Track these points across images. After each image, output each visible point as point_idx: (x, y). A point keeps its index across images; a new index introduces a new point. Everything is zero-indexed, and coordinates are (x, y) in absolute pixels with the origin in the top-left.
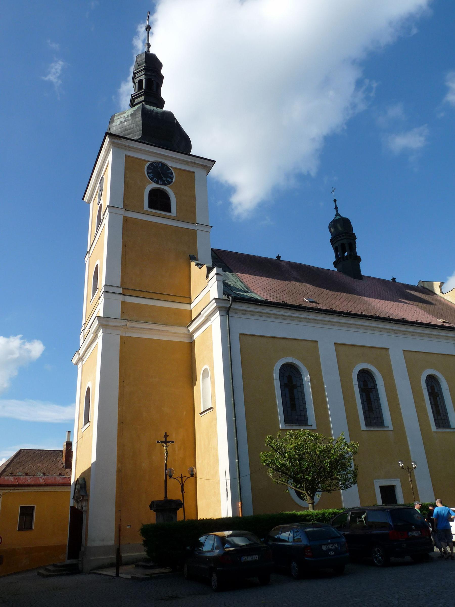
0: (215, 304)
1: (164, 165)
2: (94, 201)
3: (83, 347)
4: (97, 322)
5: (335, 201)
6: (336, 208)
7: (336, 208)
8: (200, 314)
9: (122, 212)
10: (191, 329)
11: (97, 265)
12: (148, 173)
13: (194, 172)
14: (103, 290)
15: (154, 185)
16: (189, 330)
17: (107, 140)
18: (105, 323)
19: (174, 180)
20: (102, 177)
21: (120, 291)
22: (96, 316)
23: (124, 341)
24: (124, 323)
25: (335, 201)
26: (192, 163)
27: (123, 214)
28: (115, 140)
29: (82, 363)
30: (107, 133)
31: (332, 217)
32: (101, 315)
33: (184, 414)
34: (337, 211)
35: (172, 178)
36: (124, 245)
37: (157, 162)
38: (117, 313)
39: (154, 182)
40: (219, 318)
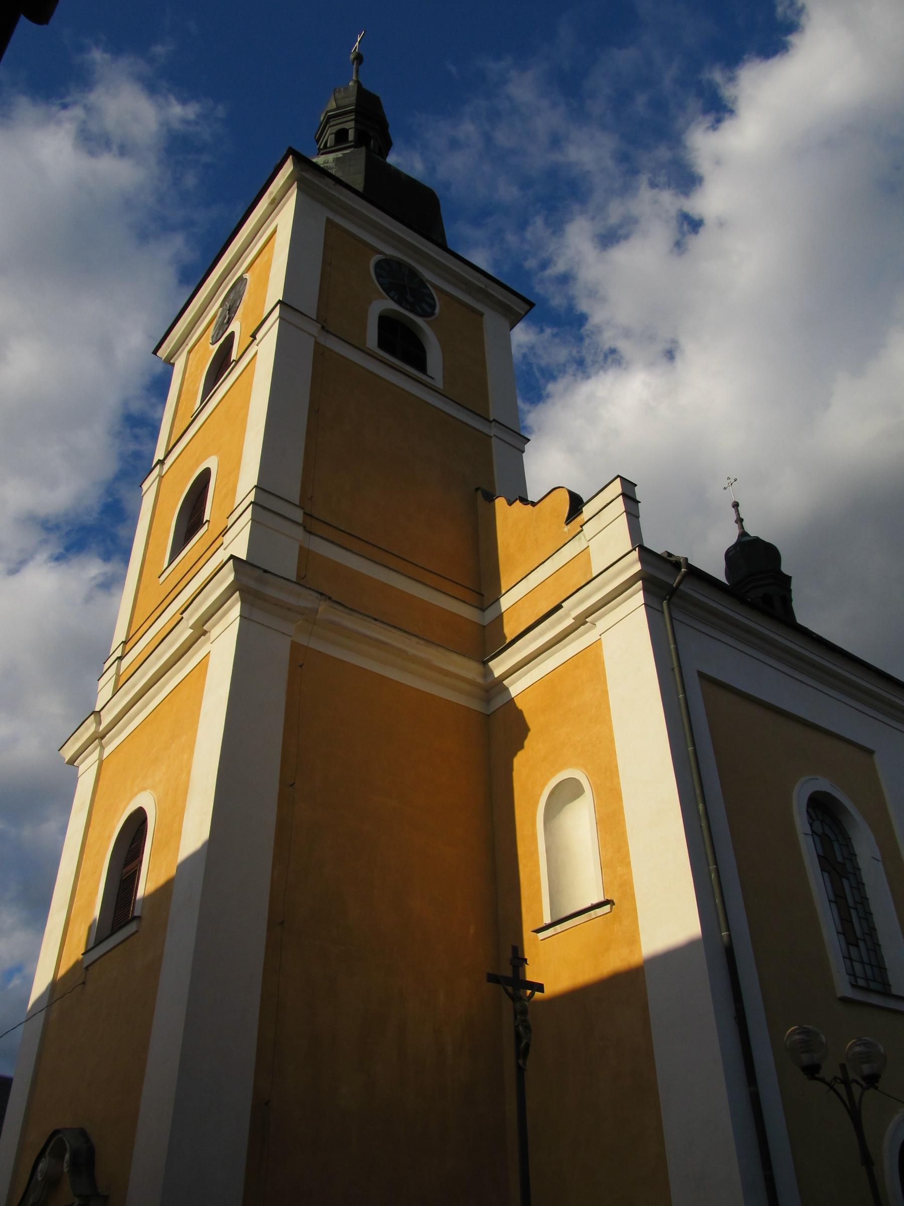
0: (638, 567)
1: (413, 274)
2: (190, 352)
3: (126, 693)
4: (228, 577)
5: (736, 505)
6: (740, 521)
7: (740, 521)
8: (558, 607)
9: (315, 329)
10: (499, 666)
11: (207, 473)
12: (378, 276)
13: (481, 315)
14: (251, 498)
15: (388, 304)
16: (490, 672)
17: (288, 168)
18: (252, 584)
19: (437, 311)
20: (241, 280)
21: (298, 515)
22: (232, 557)
23: (301, 661)
24: (307, 600)
25: (736, 505)
26: (480, 290)
27: (316, 335)
28: (307, 175)
29: (101, 753)
30: (291, 152)
31: (731, 537)
32: (243, 556)
33: (472, 931)
34: (742, 527)
35: (433, 307)
36: (314, 410)
37: (400, 264)
38: (289, 567)
39: (392, 299)
40: (641, 615)
